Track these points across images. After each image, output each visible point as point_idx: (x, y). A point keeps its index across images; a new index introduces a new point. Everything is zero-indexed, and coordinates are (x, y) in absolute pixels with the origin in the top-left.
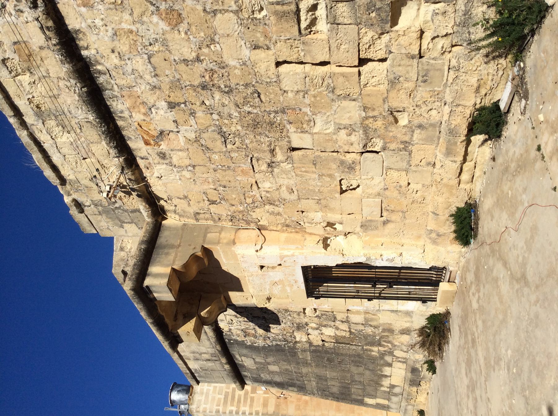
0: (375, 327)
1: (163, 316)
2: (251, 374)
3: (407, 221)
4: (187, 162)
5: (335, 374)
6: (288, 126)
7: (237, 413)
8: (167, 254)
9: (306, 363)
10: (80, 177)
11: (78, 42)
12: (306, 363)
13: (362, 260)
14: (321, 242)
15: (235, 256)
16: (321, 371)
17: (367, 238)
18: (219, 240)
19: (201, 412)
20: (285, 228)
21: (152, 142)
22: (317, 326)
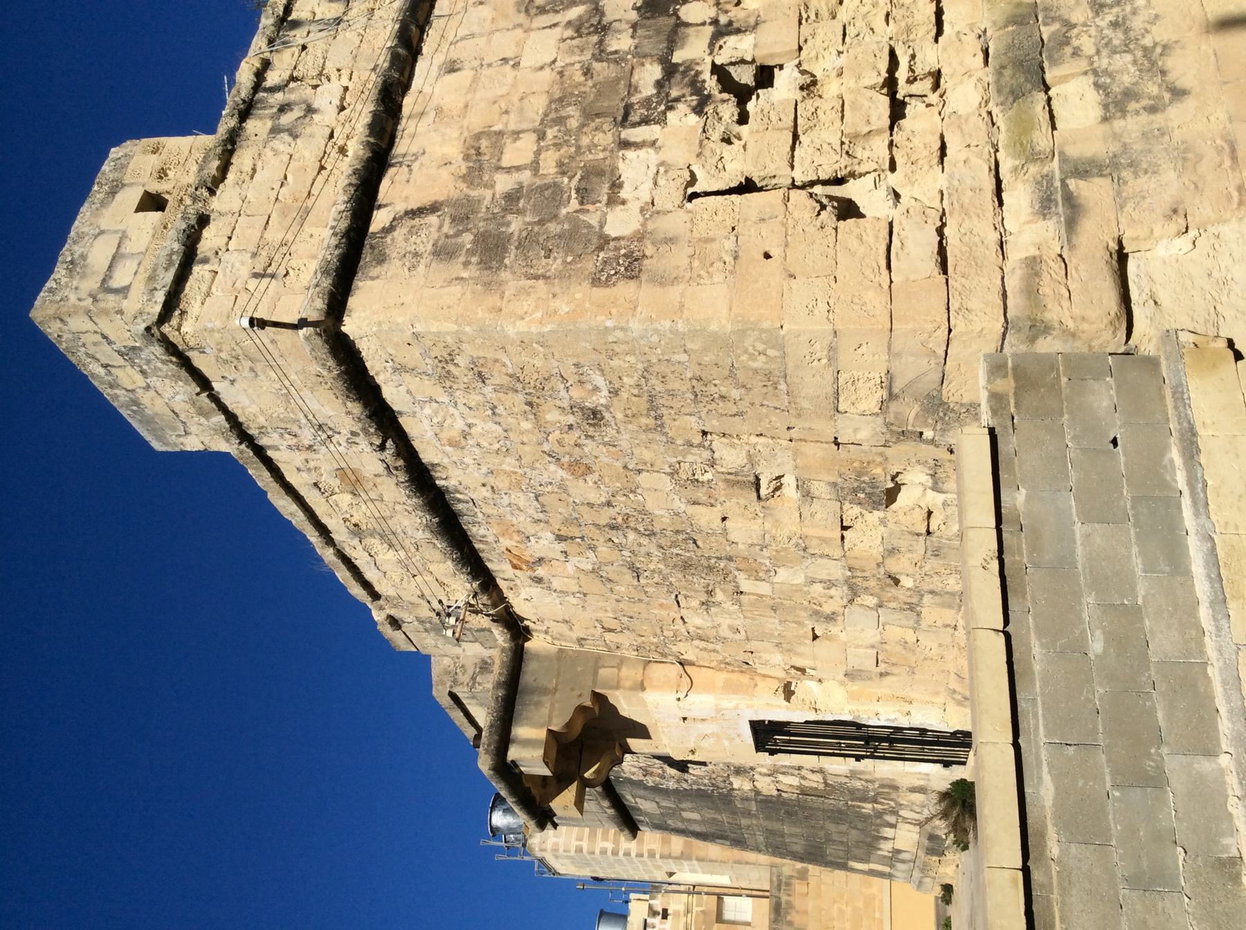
0: (867, 781)
1: (529, 788)
2: (650, 819)
3: (916, 677)
4: (576, 589)
5: (798, 830)
6: (736, 573)
7: (615, 853)
8: (538, 704)
9: (748, 814)
10: (402, 593)
11: (432, 473)
13: (847, 717)
14: (781, 690)
15: (643, 704)
16: (776, 826)
17: (855, 688)
18: (618, 682)
20: (723, 666)
21: (524, 567)
22: (769, 772)
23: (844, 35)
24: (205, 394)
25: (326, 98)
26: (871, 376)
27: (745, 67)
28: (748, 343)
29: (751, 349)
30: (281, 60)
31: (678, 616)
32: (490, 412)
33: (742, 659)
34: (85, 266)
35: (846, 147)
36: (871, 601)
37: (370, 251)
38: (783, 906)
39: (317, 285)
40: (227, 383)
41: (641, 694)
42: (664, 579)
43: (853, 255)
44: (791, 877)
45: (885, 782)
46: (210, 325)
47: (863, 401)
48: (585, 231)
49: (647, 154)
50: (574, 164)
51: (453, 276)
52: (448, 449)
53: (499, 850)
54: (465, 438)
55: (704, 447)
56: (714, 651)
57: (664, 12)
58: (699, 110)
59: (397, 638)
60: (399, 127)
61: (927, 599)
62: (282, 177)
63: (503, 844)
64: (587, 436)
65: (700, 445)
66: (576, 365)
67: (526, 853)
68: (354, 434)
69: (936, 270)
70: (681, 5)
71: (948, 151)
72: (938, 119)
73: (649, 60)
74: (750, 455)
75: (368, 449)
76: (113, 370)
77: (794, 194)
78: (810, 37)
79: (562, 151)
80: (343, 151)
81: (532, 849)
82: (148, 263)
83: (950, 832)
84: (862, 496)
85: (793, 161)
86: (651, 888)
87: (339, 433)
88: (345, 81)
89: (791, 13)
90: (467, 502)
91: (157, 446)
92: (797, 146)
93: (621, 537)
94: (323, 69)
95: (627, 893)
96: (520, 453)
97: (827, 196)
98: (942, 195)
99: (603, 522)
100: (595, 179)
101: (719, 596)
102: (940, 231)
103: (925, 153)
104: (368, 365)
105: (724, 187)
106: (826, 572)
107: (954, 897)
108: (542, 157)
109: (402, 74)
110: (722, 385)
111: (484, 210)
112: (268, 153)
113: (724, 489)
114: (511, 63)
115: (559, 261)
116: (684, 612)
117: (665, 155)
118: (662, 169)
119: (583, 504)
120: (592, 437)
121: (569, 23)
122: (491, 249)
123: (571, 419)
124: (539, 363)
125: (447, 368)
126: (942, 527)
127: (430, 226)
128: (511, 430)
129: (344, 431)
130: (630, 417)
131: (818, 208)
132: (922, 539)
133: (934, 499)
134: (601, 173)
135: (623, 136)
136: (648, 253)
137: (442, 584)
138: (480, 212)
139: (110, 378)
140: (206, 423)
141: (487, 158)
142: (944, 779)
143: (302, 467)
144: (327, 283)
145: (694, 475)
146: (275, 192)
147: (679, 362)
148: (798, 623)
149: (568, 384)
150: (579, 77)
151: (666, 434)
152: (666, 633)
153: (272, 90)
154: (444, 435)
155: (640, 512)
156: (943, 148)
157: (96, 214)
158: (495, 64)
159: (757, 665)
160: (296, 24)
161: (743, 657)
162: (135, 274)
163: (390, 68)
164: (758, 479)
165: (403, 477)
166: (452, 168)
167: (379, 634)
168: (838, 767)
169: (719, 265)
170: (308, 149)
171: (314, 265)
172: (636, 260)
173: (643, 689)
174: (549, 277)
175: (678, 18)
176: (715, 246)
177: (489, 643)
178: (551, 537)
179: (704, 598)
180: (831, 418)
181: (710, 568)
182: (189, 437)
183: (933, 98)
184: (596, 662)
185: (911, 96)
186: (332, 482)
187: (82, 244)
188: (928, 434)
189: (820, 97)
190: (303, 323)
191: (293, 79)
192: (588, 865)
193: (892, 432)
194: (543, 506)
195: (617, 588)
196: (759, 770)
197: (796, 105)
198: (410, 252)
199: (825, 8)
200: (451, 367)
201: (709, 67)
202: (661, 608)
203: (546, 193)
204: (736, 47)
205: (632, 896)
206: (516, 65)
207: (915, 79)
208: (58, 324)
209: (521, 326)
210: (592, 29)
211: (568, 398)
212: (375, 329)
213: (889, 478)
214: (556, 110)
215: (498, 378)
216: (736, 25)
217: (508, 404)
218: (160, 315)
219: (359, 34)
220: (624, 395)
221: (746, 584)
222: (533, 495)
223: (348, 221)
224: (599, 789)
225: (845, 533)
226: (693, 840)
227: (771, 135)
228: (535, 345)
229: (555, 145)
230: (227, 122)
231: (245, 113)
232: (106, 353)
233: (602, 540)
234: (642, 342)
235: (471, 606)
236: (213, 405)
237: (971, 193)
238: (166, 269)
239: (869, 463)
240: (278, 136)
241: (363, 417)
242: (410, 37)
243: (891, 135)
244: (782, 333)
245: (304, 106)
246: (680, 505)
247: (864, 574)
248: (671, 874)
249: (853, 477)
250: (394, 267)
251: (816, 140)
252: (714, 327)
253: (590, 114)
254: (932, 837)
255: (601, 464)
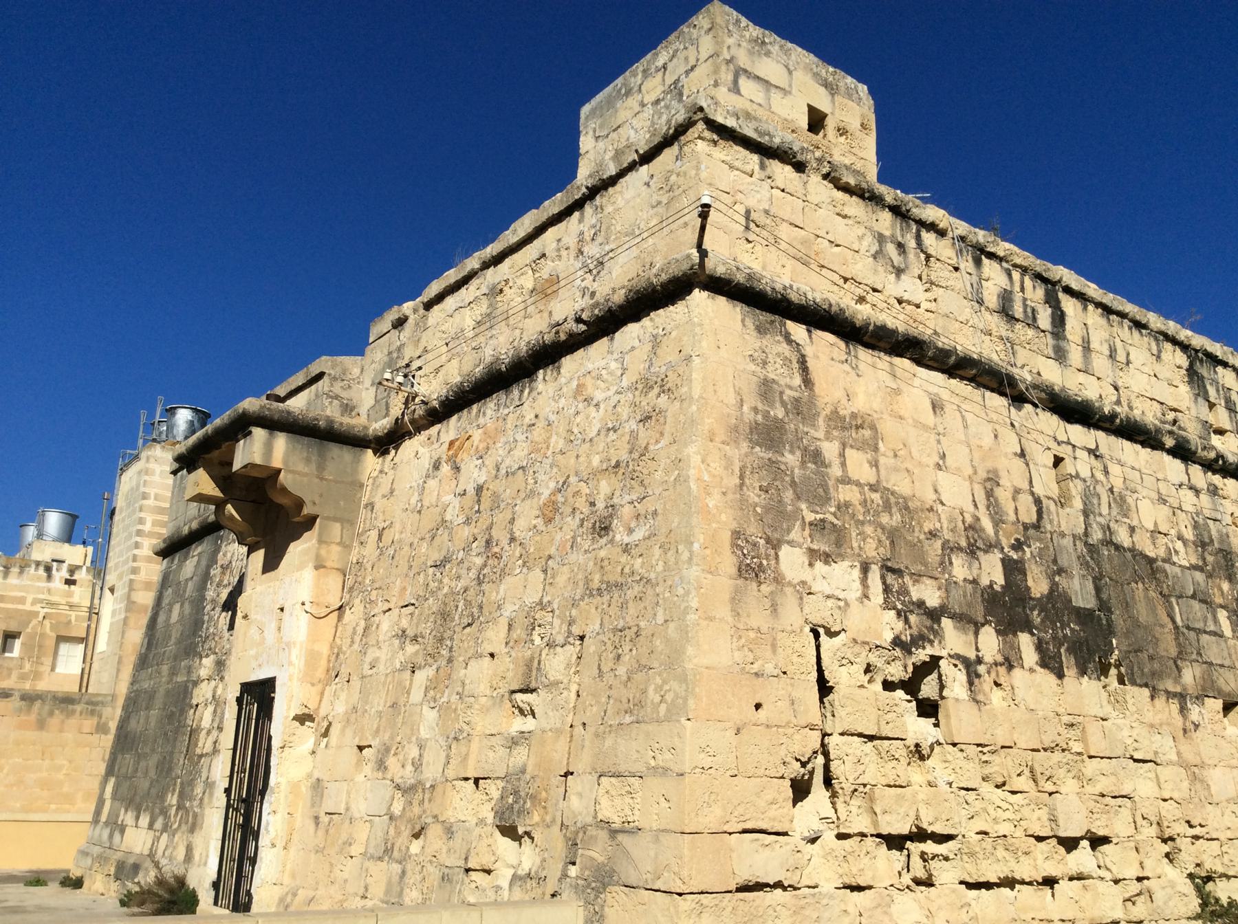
0: (201, 799)
2: (174, 570)
4: (426, 503)
5: (152, 724)
6: (434, 667)
7: (139, 533)
8: (308, 460)
9: (173, 672)
10: (429, 332)
11: (551, 367)
12: (173, 674)
14: (306, 711)
15: (301, 567)
16: (159, 701)
17: (304, 789)
18: (325, 542)
19: (147, 465)
20: (336, 651)
21: (451, 453)
23: (967, 789)
24: (636, 158)
25: (910, 287)
26: (636, 812)
27: (937, 689)
28: (674, 685)
29: (667, 687)
30: (945, 247)
31: (391, 605)
32: (610, 426)
33: (342, 671)
34: (760, 54)
35: (861, 789)
36: (397, 808)
37: (769, 320)
38: (70, 707)
39: (738, 269)
40: (647, 179)
41: (311, 565)
42: (432, 592)
43: (758, 795)
44: (100, 717)
45: (199, 818)
46: (703, 167)
47: (610, 803)
48: (785, 526)
49: (855, 590)
50: (847, 518)
51: (744, 397)
52: (575, 383)
53: (151, 415)
54: (585, 400)
55: (568, 637)
56: (353, 642)
57: (988, 612)
58: (897, 642)
59: (385, 323)
60: (882, 354)
61: (396, 868)
62: (839, 243)
63: (157, 419)
64: (582, 520)
65: (570, 633)
66: (655, 513)
67: (145, 442)
68: (593, 294)
69: (740, 880)
70: (995, 628)
71: (855, 893)
72: (887, 884)
73: (944, 595)
74: (557, 683)
75: (577, 307)
76: (660, 74)
77: (817, 735)
78: (965, 755)
79: (859, 507)
80: (861, 300)
81: (150, 447)
82: (760, 113)
83: (141, 887)
84: (510, 801)
85: (848, 735)
86: (99, 567)
87: (594, 281)
88: (925, 305)
89: (988, 736)
90: (520, 399)
91: (585, 110)
92: (863, 739)
93: (478, 550)
94: (937, 286)
95: (94, 543)
96: (568, 454)
97: (813, 768)
98: (814, 887)
99: (494, 532)
100: (833, 537)
101: (411, 649)
102: (779, 885)
103: (854, 871)
104: (661, 311)
105: (824, 664)
106: (431, 762)
107: (68, 891)
108: (854, 487)
109: (931, 359)
110: (631, 656)
111: (806, 429)
112: (861, 231)
113: (523, 657)
114: (941, 462)
115: (757, 499)
116: (396, 612)
117: (855, 606)
118: (842, 604)
119: (514, 513)
120: (582, 525)
121: (978, 519)
122: (768, 434)
123: (600, 505)
124: (658, 476)
125: (655, 386)
126: (473, 885)
127: (791, 378)
128: (592, 446)
129: (595, 285)
130: (601, 564)
131: (803, 759)
132: (462, 863)
133: (503, 876)
134: (838, 544)
135: (873, 566)
136: (763, 587)
137: (437, 371)
138: (804, 426)
139: (653, 70)
140: (607, 157)
141: (854, 435)
142: (200, 882)
143: (561, 244)
144: (740, 278)
145: (539, 626)
146: (824, 235)
147: (655, 615)
148: (378, 731)
149: (636, 504)
150: (928, 526)
151: (582, 599)
152: (374, 593)
153: (918, 237)
154: (589, 381)
155: (503, 570)
156: (859, 888)
157: (808, 68)
158: (939, 446)
159: (334, 687)
160: (978, 263)
161: (344, 671)
162: (751, 101)
163: (937, 348)
164: (532, 691)
165: (548, 338)
166: (844, 401)
167: (390, 307)
168: (220, 769)
169: (750, 658)
170: (863, 268)
171: (757, 267)
172: (757, 575)
173: (317, 568)
174: (741, 489)
175: (983, 625)
176: (769, 654)
177: (372, 415)
178: (481, 481)
179: (410, 633)
180: (594, 769)
181: (441, 640)
182: (593, 140)
183: (907, 879)
184: (348, 521)
185: (909, 856)
186: (547, 268)
187: (780, 53)
188: (573, 871)
189: (909, 764)
190: (703, 254)
191: (928, 257)
192: (129, 505)
193: (577, 833)
194: (513, 474)
195: (425, 545)
196: (220, 686)
197: (902, 739)
198: (767, 357)
199: (992, 770)
200: (656, 390)
201: (937, 654)
202: (401, 588)
203: (821, 490)
204: (956, 678)
205: (90, 549)
206: (939, 467)
207: (925, 860)
208: (706, 26)
209: (696, 460)
210: (972, 541)
211: (623, 503)
212: (696, 320)
213: (528, 829)
214: (897, 503)
215: (644, 435)
216: (976, 681)
217: (618, 443)
218: (714, 121)
219: (968, 321)
220: (624, 559)
221: (422, 676)
222: (525, 464)
223: (797, 302)
224: (212, 518)
225: (471, 781)
226: (149, 614)
227: (873, 714)
228: (676, 472)
229: (865, 501)
230: (889, 194)
231: (898, 211)
232: (677, 69)
233: (476, 531)
234: (677, 578)
235: (414, 399)
236: (625, 165)
237: (815, 917)
238: (756, 130)
239: (545, 808)
240: (875, 241)
241: (610, 304)
242: (966, 368)
243: (872, 835)
244: (683, 720)
245: (903, 266)
246: (508, 610)
247: (426, 801)
248: (112, 590)
249: (531, 791)
250: (753, 341)
251: (868, 759)
252: (690, 650)
253: (893, 536)
254: (136, 868)
255: (554, 534)
